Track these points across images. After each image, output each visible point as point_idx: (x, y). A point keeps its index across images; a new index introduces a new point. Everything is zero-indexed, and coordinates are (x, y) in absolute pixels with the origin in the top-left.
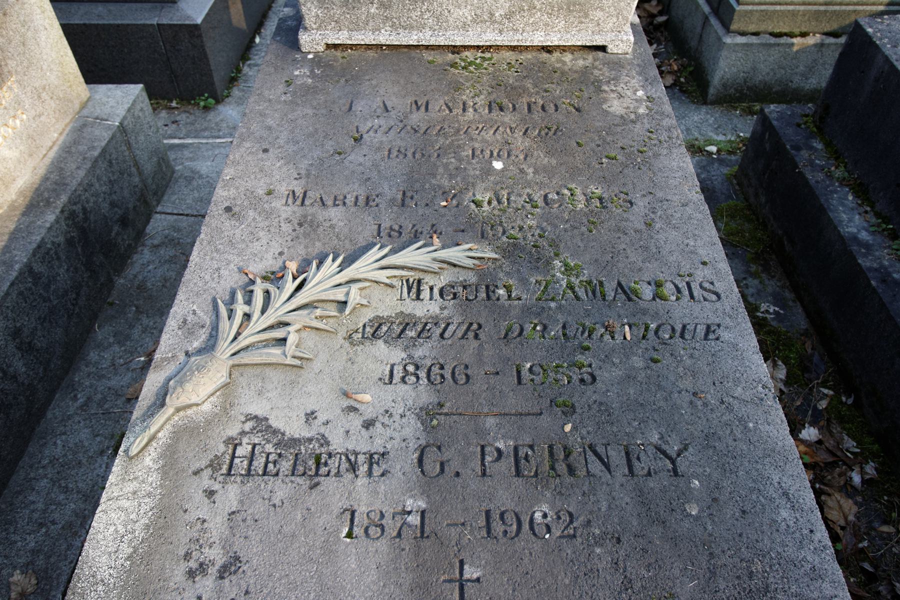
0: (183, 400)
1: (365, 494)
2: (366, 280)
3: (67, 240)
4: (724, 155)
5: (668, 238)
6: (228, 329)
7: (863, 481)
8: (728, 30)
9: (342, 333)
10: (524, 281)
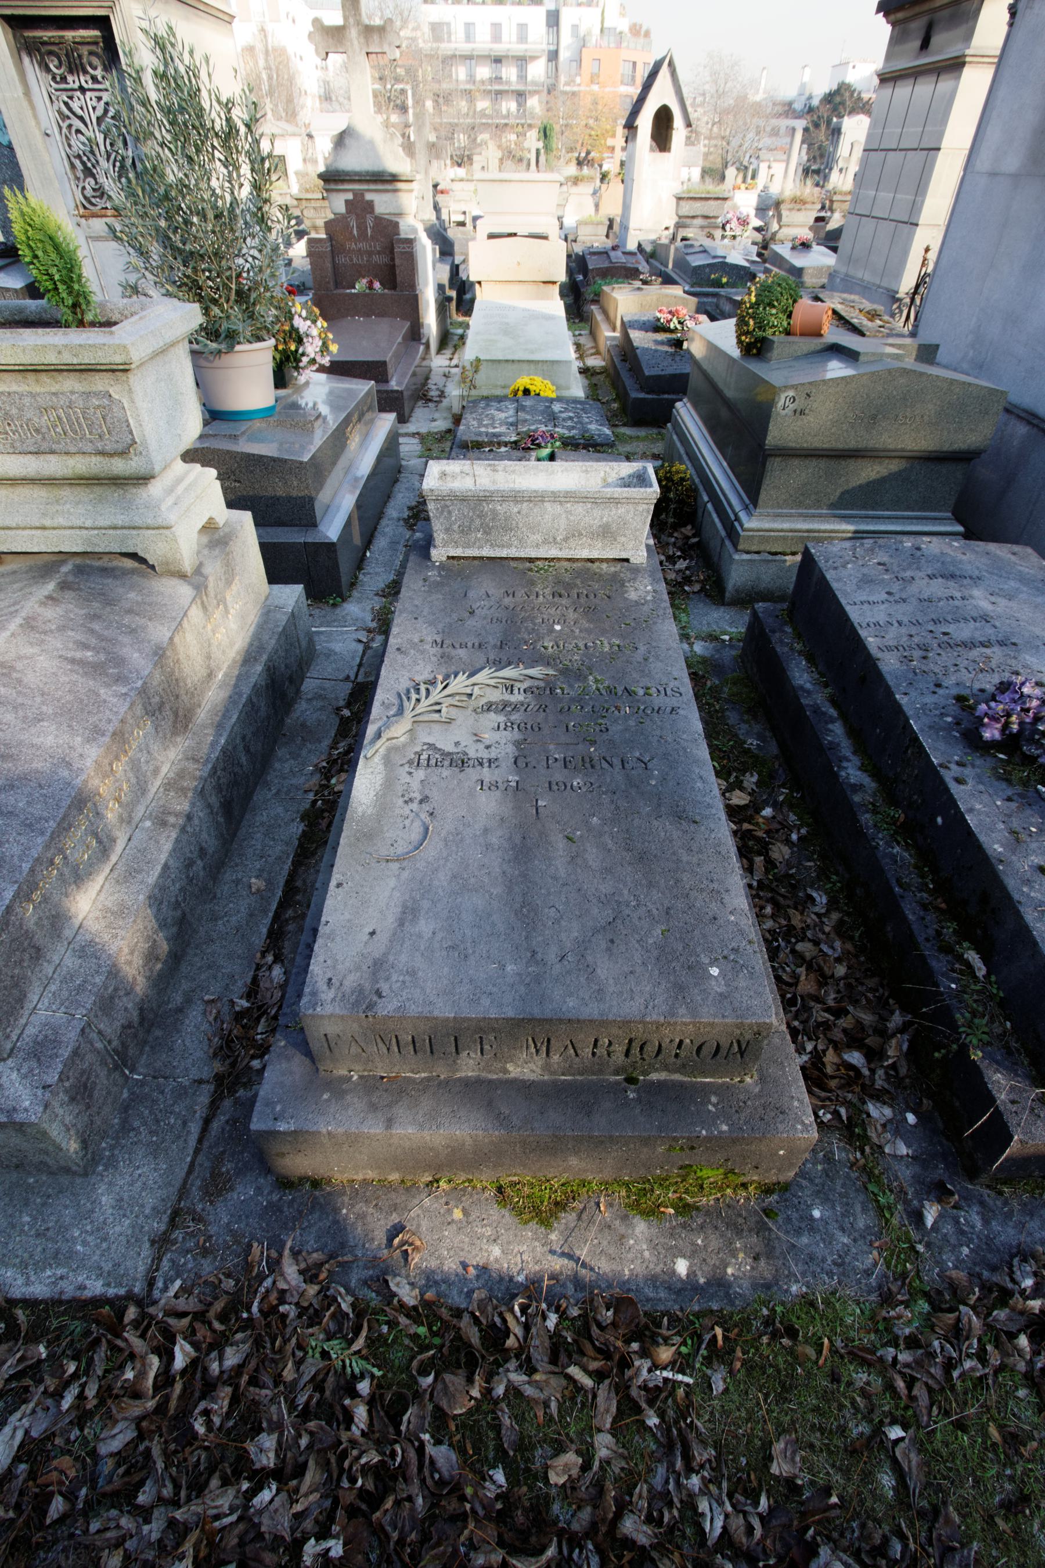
0: (390, 735)
4: (734, 642)
5: (656, 667)
6: (408, 706)
7: (799, 839)
8: (737, 550)
9: (471, 708)
10: (571, 686)
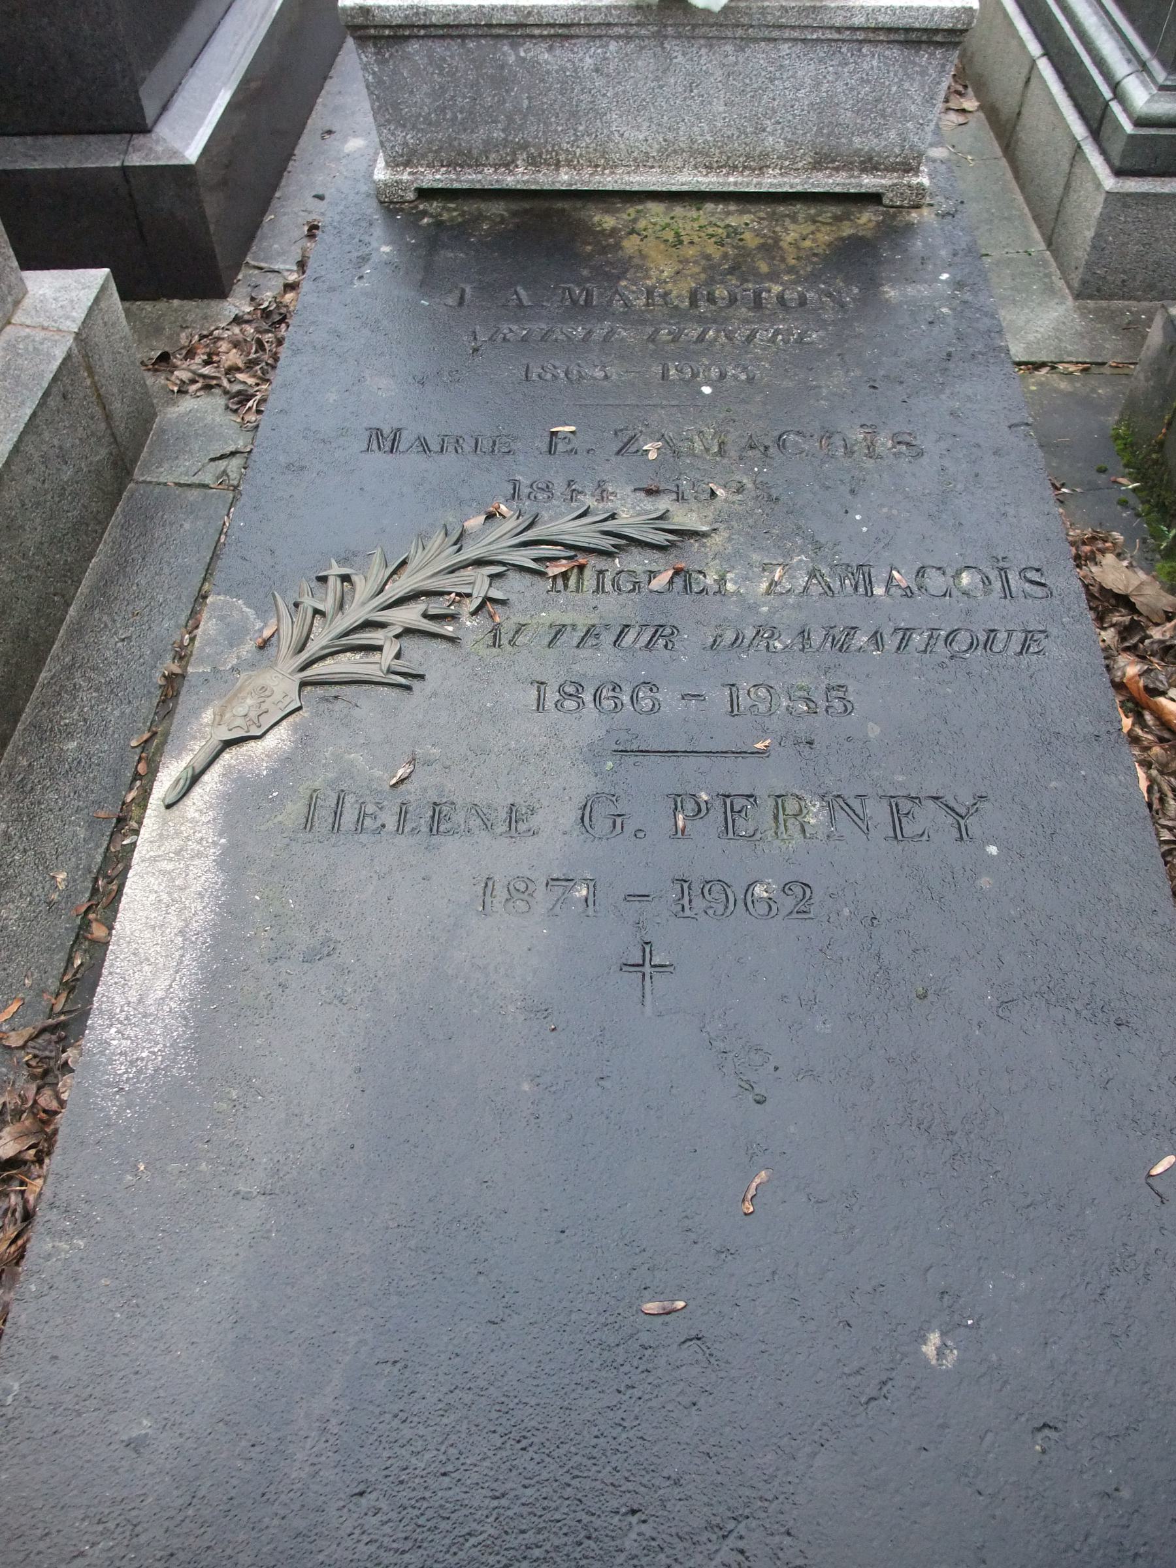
1: (506, 858)
2: (504, 564)
3: (1089, 290)
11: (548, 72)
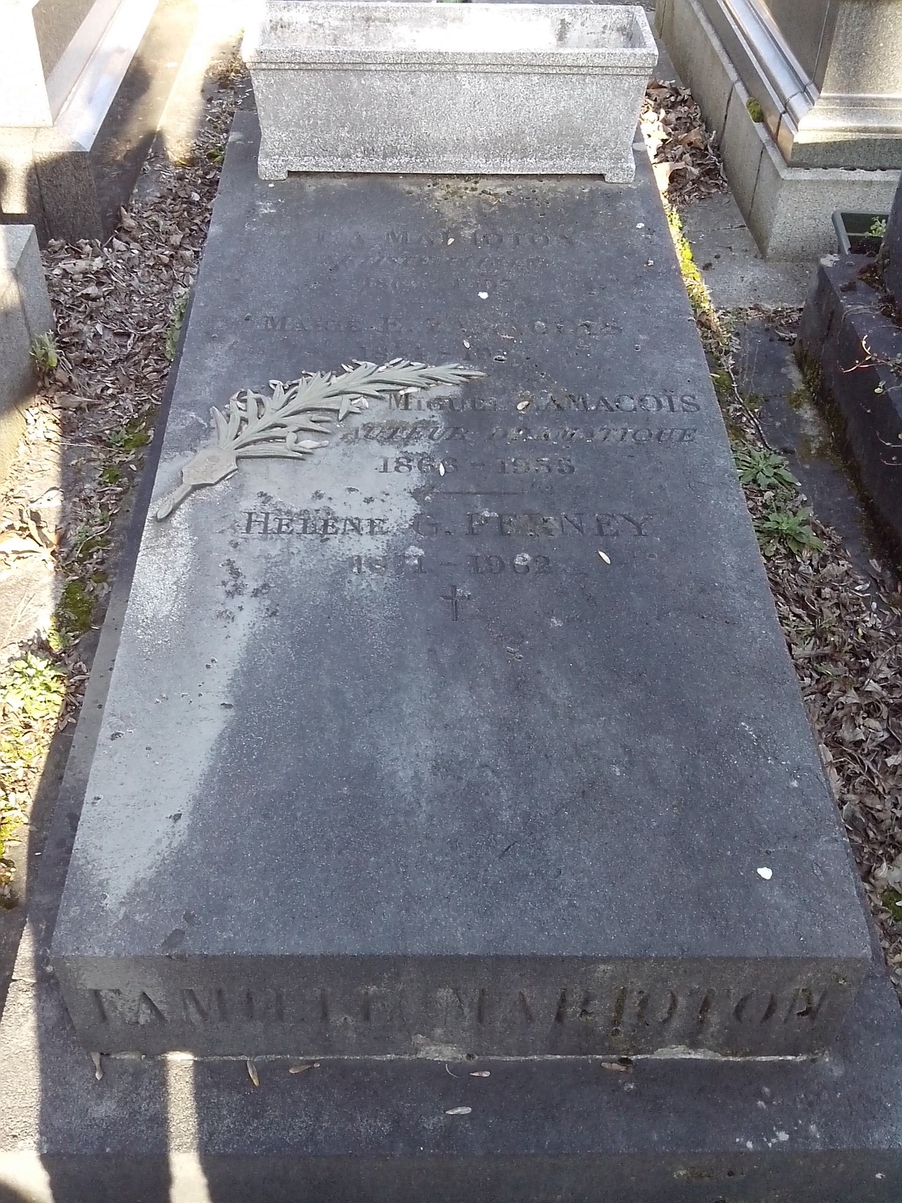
11: (380, 94)
